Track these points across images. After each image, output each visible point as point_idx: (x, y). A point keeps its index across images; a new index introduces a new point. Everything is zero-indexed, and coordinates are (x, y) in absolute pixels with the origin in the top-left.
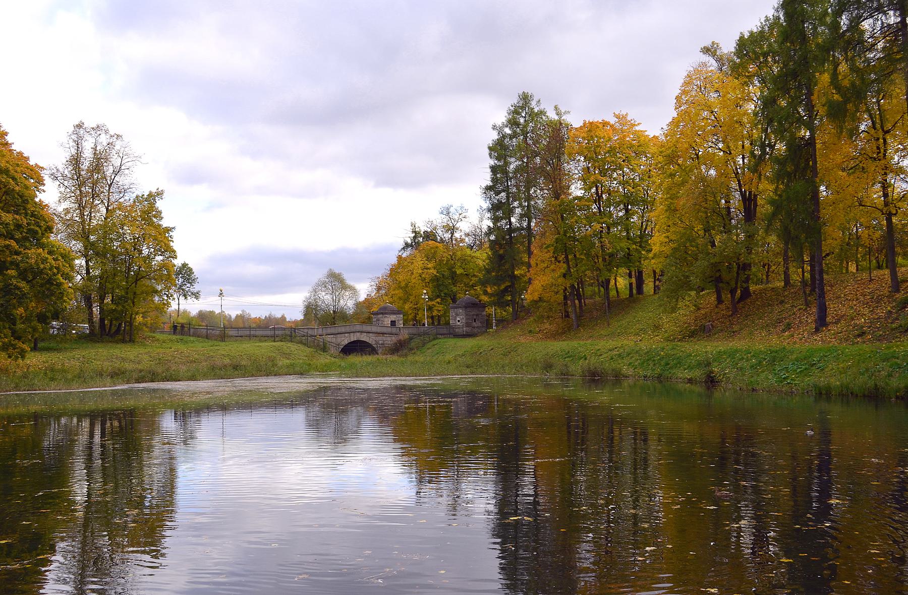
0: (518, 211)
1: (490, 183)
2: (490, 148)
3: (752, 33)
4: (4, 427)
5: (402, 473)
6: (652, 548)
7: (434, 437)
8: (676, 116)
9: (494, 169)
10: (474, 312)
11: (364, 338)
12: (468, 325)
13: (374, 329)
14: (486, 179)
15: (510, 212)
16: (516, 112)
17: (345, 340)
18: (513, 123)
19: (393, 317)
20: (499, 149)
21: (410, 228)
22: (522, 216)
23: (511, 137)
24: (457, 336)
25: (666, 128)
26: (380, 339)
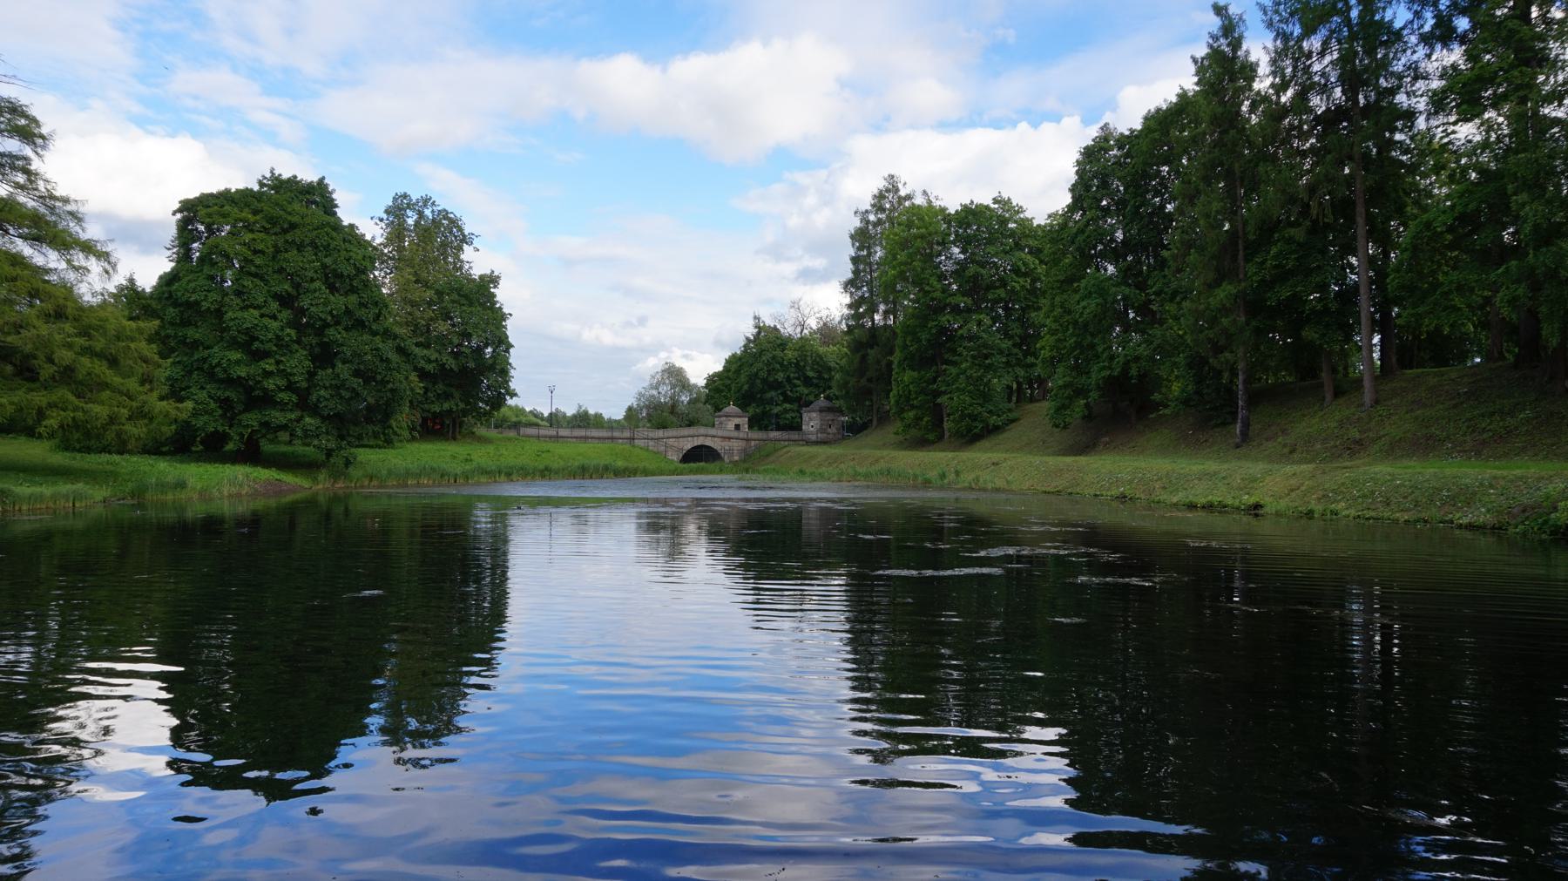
0: (882, 307)
1: (850, 275)
2: (852, 237)
3: (1132, 131)
4: (1334, 5)
5: (160, 702)
6: (1076, 620)
7: (768, 549)
8: (1035, 223)
9: (855, 260)
10: (830, 416)
11: (708, 442)
12: (822, 430)
13: (720, 433)
14: (847, 272)
15: (873, 309)
16: (880, 196)
17: (688, 445)
18: (878, 208)
19: (737, 421)
20: (862, 237)
21: (752, 322)
22: (886, 313)
23: (875, 225)
24: (808, 443)
25: (813, 324)
26: (727, 444)
